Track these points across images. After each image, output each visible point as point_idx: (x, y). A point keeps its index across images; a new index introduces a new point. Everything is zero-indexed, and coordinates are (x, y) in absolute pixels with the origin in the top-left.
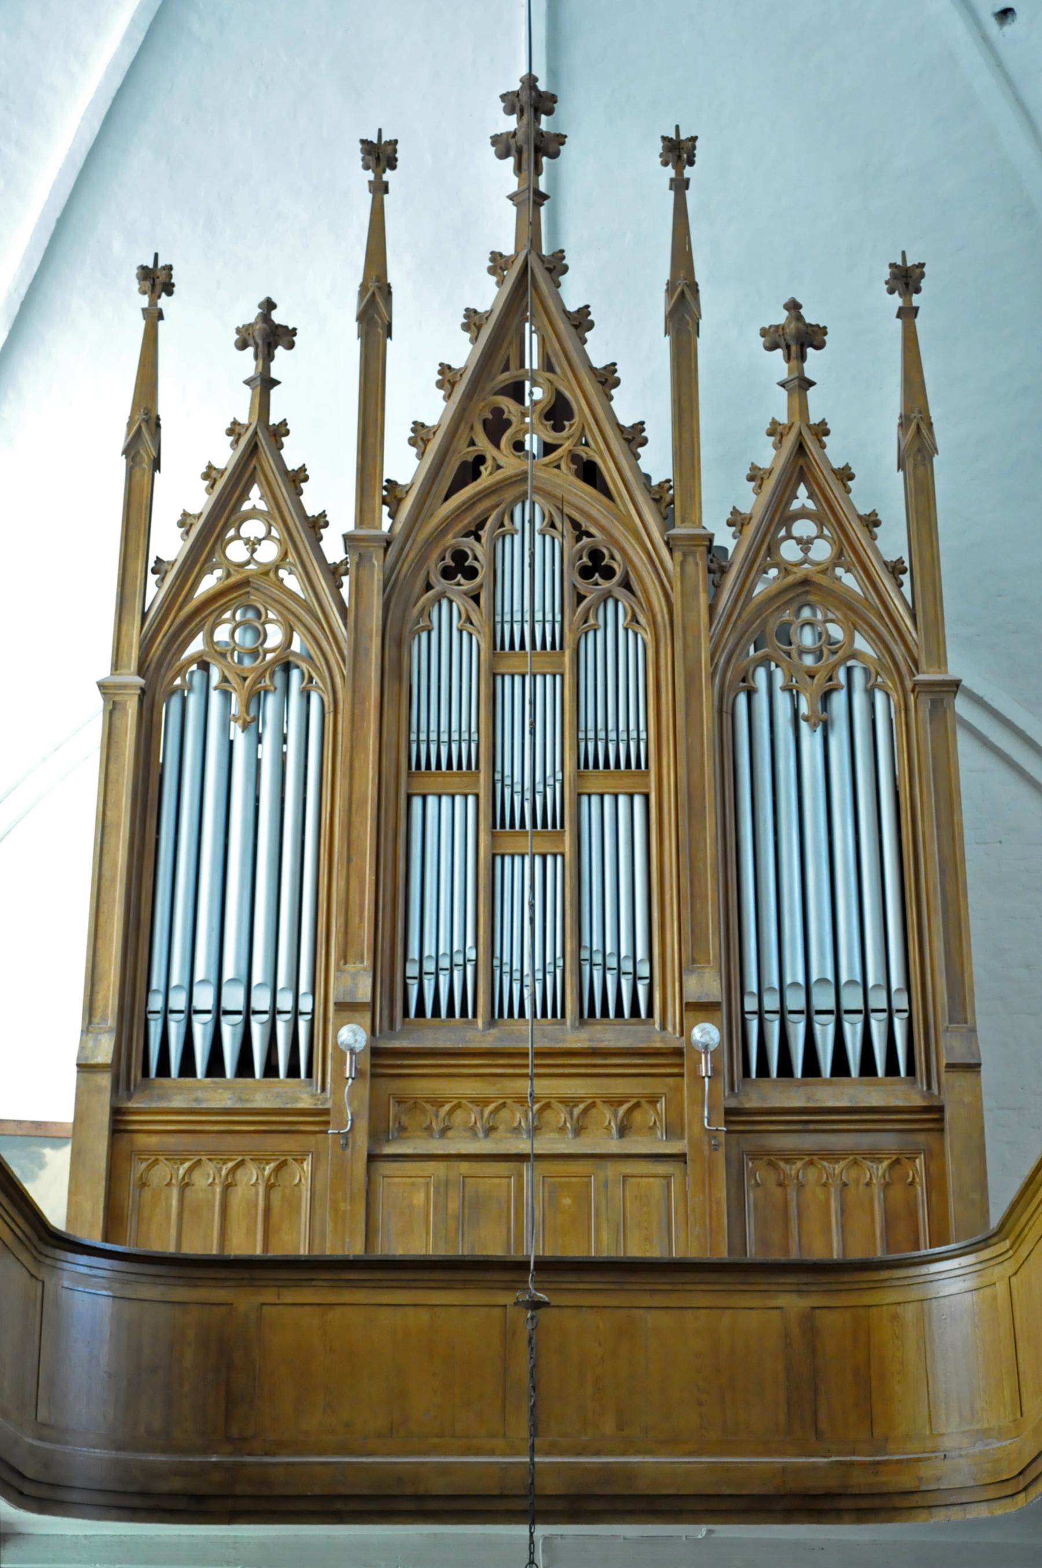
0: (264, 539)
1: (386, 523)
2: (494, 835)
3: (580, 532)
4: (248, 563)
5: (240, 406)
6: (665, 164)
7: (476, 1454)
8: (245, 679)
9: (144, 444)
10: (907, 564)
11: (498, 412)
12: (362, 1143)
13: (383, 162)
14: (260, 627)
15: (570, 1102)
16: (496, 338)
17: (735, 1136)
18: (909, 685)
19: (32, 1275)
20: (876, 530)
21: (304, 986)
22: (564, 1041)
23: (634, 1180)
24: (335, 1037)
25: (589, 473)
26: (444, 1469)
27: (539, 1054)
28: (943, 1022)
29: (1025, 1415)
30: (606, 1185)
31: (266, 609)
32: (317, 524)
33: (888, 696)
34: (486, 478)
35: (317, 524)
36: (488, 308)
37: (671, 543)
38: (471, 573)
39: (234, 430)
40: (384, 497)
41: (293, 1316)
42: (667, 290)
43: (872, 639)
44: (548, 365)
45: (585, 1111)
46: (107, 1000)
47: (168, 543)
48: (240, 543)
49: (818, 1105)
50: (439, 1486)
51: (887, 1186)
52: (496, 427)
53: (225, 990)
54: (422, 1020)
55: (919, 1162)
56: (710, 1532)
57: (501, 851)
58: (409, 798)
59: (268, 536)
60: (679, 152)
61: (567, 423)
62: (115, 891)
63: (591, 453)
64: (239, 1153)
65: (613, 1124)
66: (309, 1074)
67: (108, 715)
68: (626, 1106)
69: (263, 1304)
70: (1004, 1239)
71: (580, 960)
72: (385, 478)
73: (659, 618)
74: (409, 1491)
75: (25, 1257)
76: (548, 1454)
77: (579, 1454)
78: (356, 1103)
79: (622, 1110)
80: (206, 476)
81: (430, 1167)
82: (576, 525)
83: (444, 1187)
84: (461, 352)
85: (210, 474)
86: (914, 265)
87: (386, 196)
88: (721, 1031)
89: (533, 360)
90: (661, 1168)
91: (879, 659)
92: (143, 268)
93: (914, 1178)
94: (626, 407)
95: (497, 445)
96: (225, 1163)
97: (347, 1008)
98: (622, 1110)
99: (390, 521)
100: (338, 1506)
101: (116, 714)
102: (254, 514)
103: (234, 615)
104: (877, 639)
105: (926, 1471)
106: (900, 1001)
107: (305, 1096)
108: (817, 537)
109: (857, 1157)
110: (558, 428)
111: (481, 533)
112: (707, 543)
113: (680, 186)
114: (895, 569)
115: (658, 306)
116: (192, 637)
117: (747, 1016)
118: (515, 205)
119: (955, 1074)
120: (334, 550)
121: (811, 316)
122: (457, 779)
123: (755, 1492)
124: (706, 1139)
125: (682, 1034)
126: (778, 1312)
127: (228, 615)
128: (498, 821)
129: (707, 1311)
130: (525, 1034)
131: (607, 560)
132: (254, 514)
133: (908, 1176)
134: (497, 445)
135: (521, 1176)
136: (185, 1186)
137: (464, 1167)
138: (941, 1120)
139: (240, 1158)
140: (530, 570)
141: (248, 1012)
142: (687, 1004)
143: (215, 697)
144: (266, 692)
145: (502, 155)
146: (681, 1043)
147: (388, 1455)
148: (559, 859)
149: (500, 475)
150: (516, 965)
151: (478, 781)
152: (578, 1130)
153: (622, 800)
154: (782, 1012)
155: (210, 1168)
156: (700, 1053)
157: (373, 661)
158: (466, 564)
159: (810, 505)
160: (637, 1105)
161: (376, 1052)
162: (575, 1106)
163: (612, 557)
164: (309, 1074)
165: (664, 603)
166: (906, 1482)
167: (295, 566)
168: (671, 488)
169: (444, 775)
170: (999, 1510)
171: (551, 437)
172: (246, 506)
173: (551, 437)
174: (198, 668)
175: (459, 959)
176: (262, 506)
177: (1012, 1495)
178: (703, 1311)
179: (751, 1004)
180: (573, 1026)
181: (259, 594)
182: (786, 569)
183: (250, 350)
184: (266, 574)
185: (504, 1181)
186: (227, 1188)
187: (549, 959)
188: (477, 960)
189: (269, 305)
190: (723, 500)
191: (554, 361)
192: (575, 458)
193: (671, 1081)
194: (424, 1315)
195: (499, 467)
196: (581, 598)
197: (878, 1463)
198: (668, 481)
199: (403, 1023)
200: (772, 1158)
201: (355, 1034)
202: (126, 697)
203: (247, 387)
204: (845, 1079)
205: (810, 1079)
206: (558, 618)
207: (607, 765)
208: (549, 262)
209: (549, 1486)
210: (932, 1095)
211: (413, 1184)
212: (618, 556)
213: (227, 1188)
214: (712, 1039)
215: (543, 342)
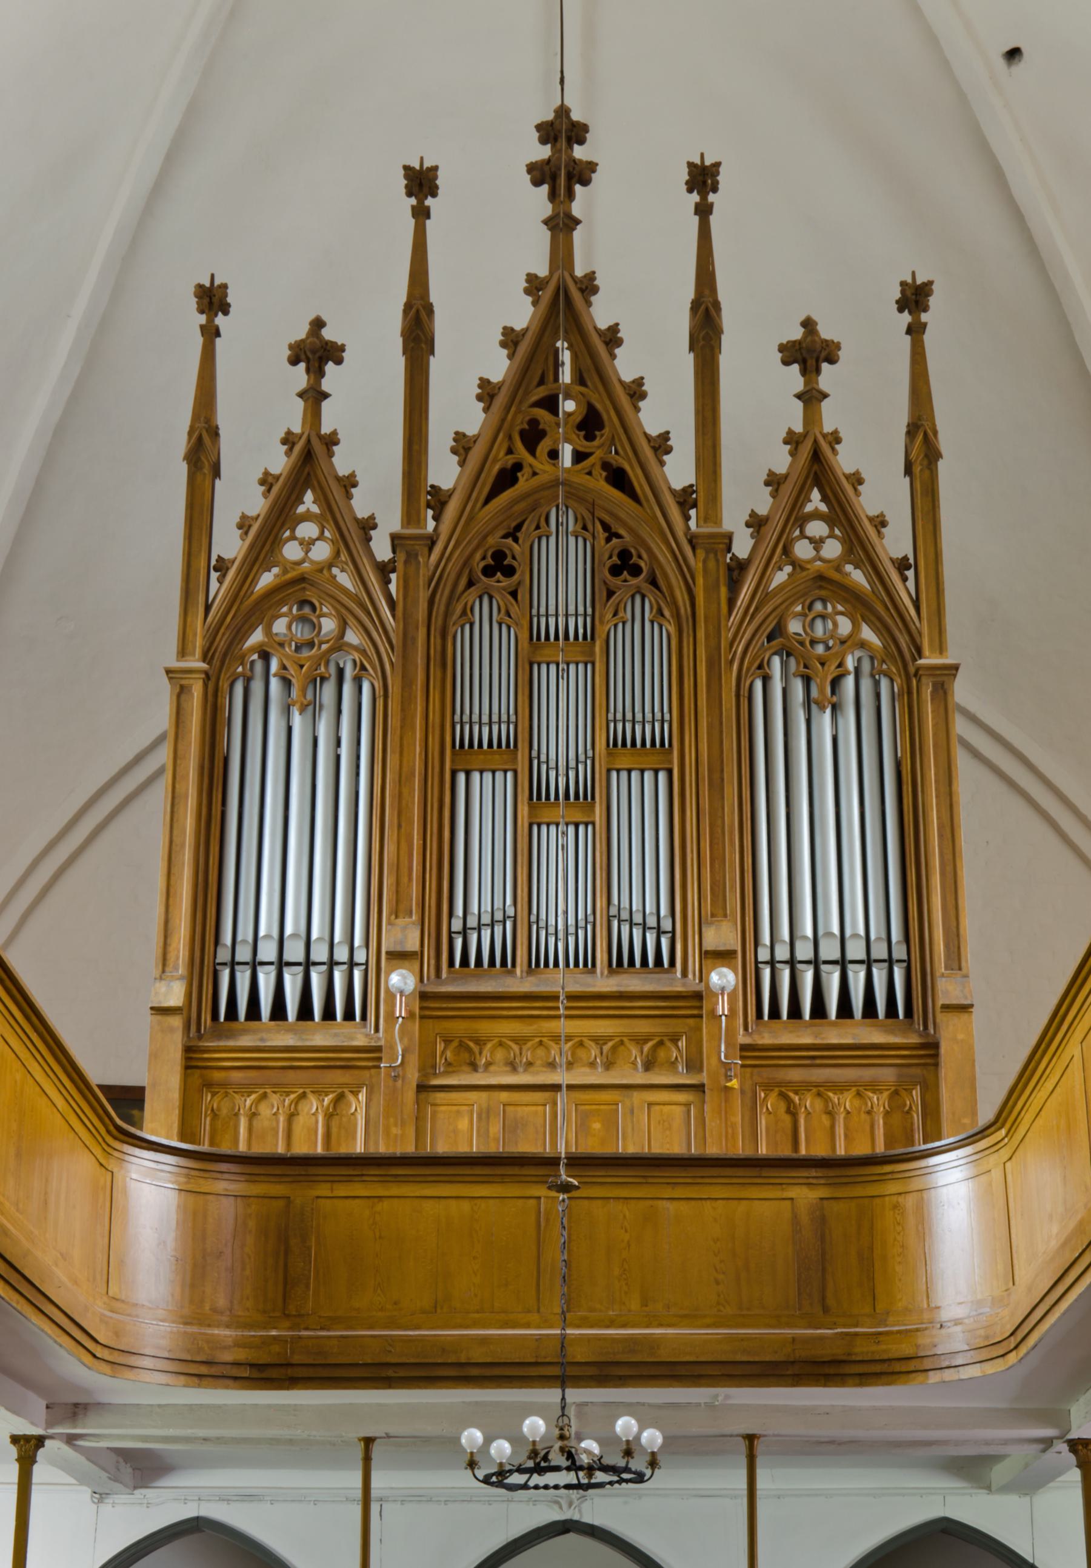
0: (317, 539)
1: (431, 525)
2: (531, 806)
3: (611, 535)
4: (303, 561)
5: (293, 416)
6: (690, 191)
7: (513, 1327)
8: (302, 666)
9: (203, 455)
10: (912, 561)
11: (534, 422)
12: (413, 1076)
13: (426, 189)
14: (315, 620)
15: (599, 1040)
16: (532, 352)
17: (749, 1070)
18: (912, 670)
19: (101, 1165)
20: (883, 530)
21: (358, 941)
22: (594, 986)
23: (657, 1108)
24: (387, 982)
25: (618, 478)
26: (484, 1341)
27: (571, 997)
28: (940, 966)
29: (1017, 1283)
30: (632, 1112)
31: (321, 604)
32: (367, 526)
33: (892, 681)
34: (524, 483)
35: (367, 526)
36: (524, 325)
37: (694, 541)
38: (510, 572)
39: (289, 440)
40: (428, 501)
41: (343, 1205)
42: (692, 309)
43: (878, 629)
44: (580, 378)
45: (614, 1049)
46: (179, 952)
47: (228, 543)
48: (296, 543)
49: (825, 1042)
50: (478, 1355)
51: (887, 1114)
52: (533, 436)
53: (286, 944)
54: (465, 969)
55: (916, 1093)
56: (727, 1397)
57: (539, 820)
58: (454, 774)
59: (321, 537)
60: (703, 178)
61: (597, 433)
62: (184, 855)
63: (620, 460)
64: (301, 1086)
65: (639, 1060)
66: (364, 1017)
67: (175, 698)
68: (650, 1044)
69: (318, 1197)
70: (1000, 1128)
71: (609, 916)
72: (429, 483)
73: (682, 611)
74: (452, 1359)
75: (98, 1151)
76: (578, 1327)
77: (607, 1327)
78: (406, 1041)
79: (647, 1048)
80: (262, 482)
81: (473, 1096)
82: (606, 527)
83: (486, 1115)
84: (498, 367)
85: (267, 481)
86: (923, 283)
87: (428, 222)
88: (736, 974)
89: (566, 376)
90: (682, 1097)
91: (884, 647)
92: (200, 286)
93: (911, 1107)
94: (651, 418)
95: (532, 451)
96: (288, 1095)
97: (399, 957)
98: (647, 1048)
99: (434, 523)
100: (390, 1373)
101: (183, 697)
102: (307, 517)
103: (291, 609)
104: (882, 628)
105: (923, 1340)
106: (899, 952)
107: (359, 1036)
108: (828, 537)
109: (861, 1089)
110: (590, 437)
111: (518, 534)
112: (727, 541)
113: (704, 211)
114: (902, 565)
115: (681, 324)
116: (253, 629)
117: (760, 965)
118: (550, 229)
119: (950, 1015)
120: (382, 550)
121: (825, 332)
122: (497, 757)
123: (767, 1359)
124: (723, 1070)
125: (701, 980)
126: (788, 1203)
127: (285, 609)
128: (536, 800)
129: (724, 1202)
130: (560, 981)
131: (635, 559)
132: (307, 517)
133: (905, 1105)
134: (532, 451)
135: (555, 1104)
136: (253, 1116)
137: (504, 1096)
138: (936, 1056)
139: (301, 1091)
140: (562, 574)
141: (308, 964)
142: (707, 952)
143: (274, 683)
144: (323, 679)
145: (537, 183)
146: (701, 987)
147: (432, 1328)
148: (590, 828)
149: (535, 481)
150: (552, 921)
151: (516, 758)
152: (608, 1065)
153: (648, 775)
154: (792, 962)
155: (274, 1099)
156: (716, 995)
157: (420, 649)
158: (505, 563)
159: (823, 507)
160: (661, 1043)
161: (424, 996)
162: (605, 1044)
163: (640, 557)
164: (364, 1017)
165: (686, 597)
166: (906, 1350)
167: (347, 564)
168: (694, 492)
169: (485, 753)
170: (990, 1368)
171: (585, 446)
172: (301, 509)
173: (585, 446)
174: (259, 657)
175: (499, 916)
176: (315, 509)
177: (1003, 1356)
178: (720, 1202)
179: (764, 955)
180: (602, 974)
181: (314, 589)
182: (798, 565)
183: (302, 366)
184: (321, 571)
185: (540, 1108)
186: (291, 1117)
187: (581, 916)
188: (515, 917)
189: (318, 324)
190: (742, 499)
191: (585, 375)
192: (606, 466)
193: (691, 1021)
194: (466, 1205)
195: (535, 474)
196: (610, 594)
197: (880, 1333)
198: (691, 486)
199: (449, 972)
200: (783, 1089)
201: (404, 977)
202: (191, 682)
203: (300, 400)
204: (849, 1021)
205: (817, 1021)
206: (589, 611)
207: (634, 744)
208: (581, 281)
209: (579, 1354)
210: (928, 1035)
211: (458, 1112)
212: (645, 556)
213: (291, 1117)
214: (728, 981)
215: (575, 358)
